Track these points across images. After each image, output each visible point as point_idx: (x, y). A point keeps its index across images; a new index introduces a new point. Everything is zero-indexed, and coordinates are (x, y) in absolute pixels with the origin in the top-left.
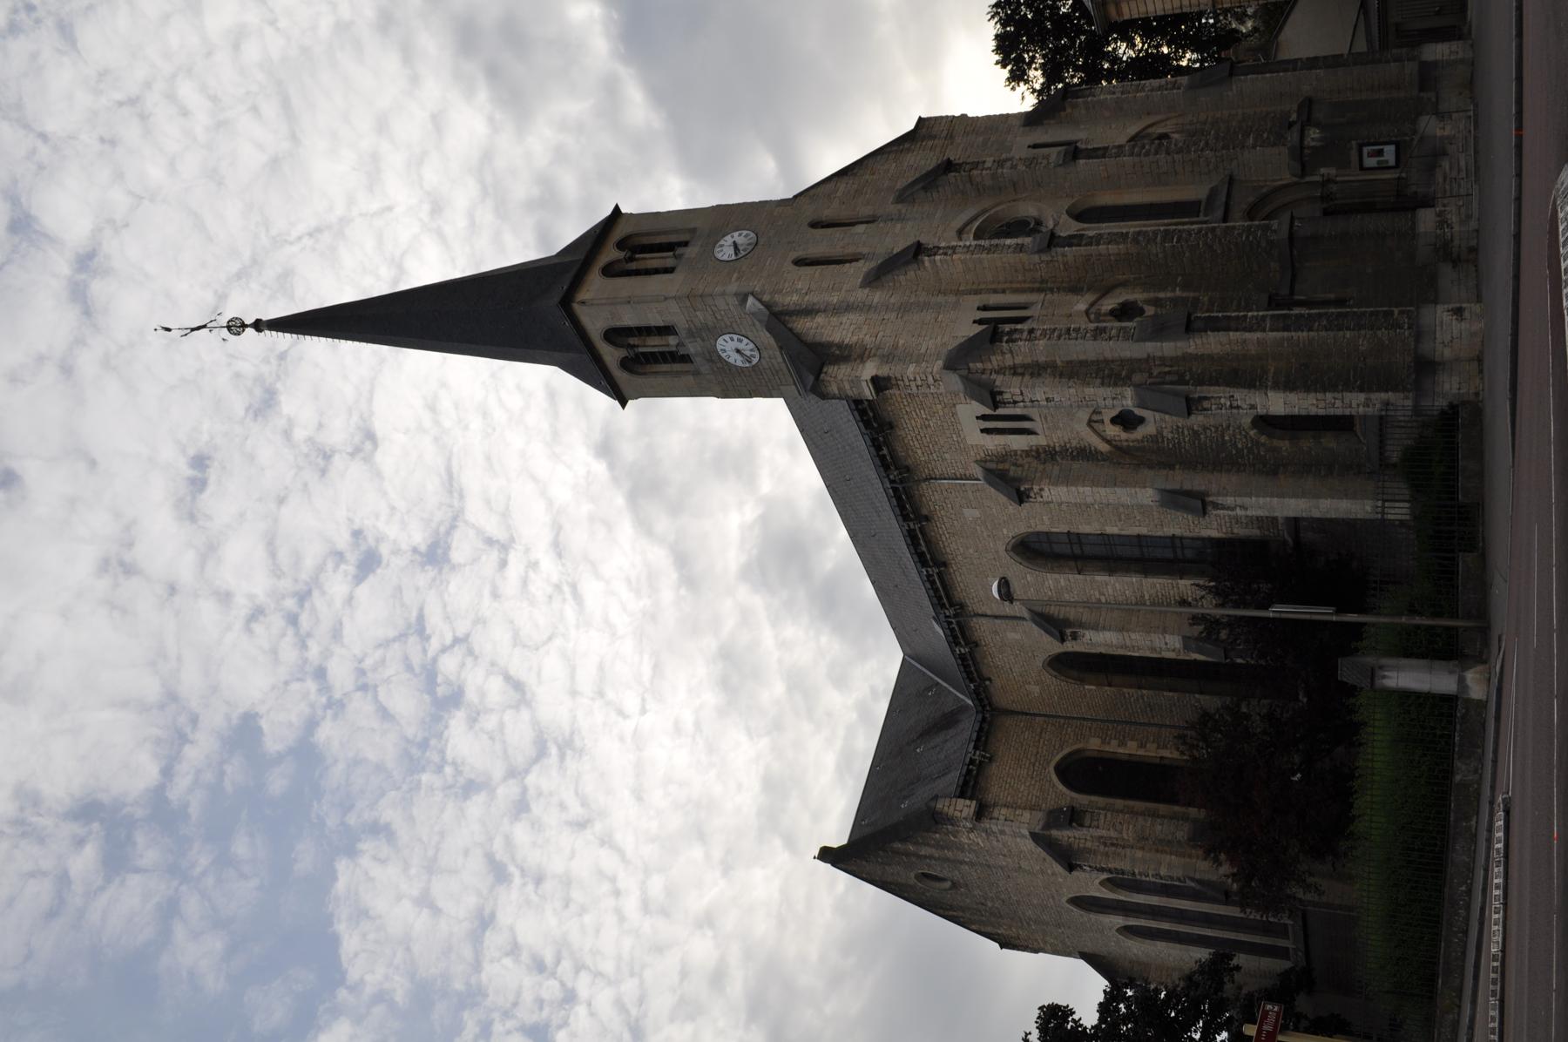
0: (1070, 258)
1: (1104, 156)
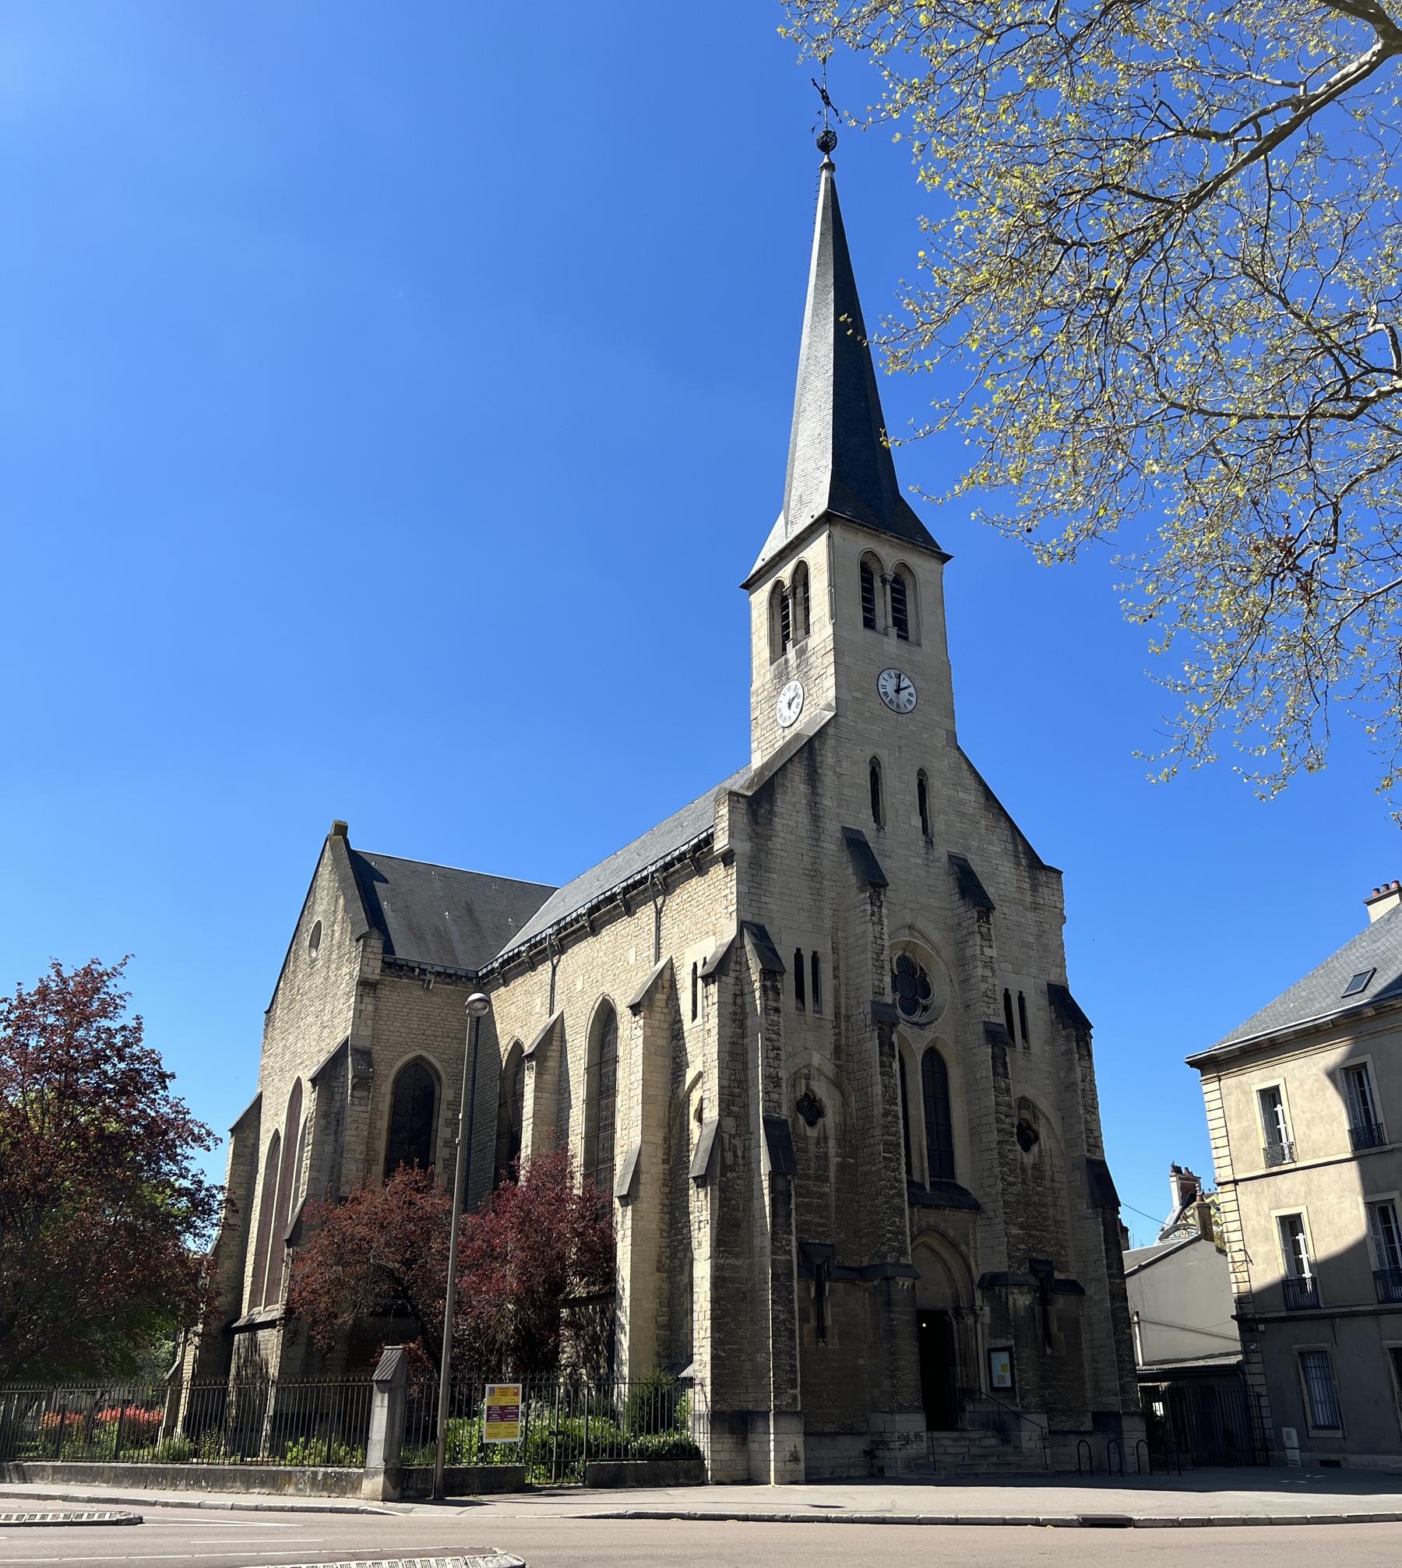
0: (869, 1045)
1: (995, 1074)
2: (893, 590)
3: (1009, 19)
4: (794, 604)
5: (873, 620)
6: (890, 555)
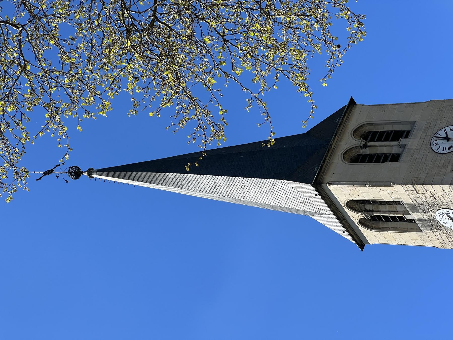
2: (372, 140)
3: (16, 54)
4: (378, 211)
5: (393, 155)
6: (347, 141)
